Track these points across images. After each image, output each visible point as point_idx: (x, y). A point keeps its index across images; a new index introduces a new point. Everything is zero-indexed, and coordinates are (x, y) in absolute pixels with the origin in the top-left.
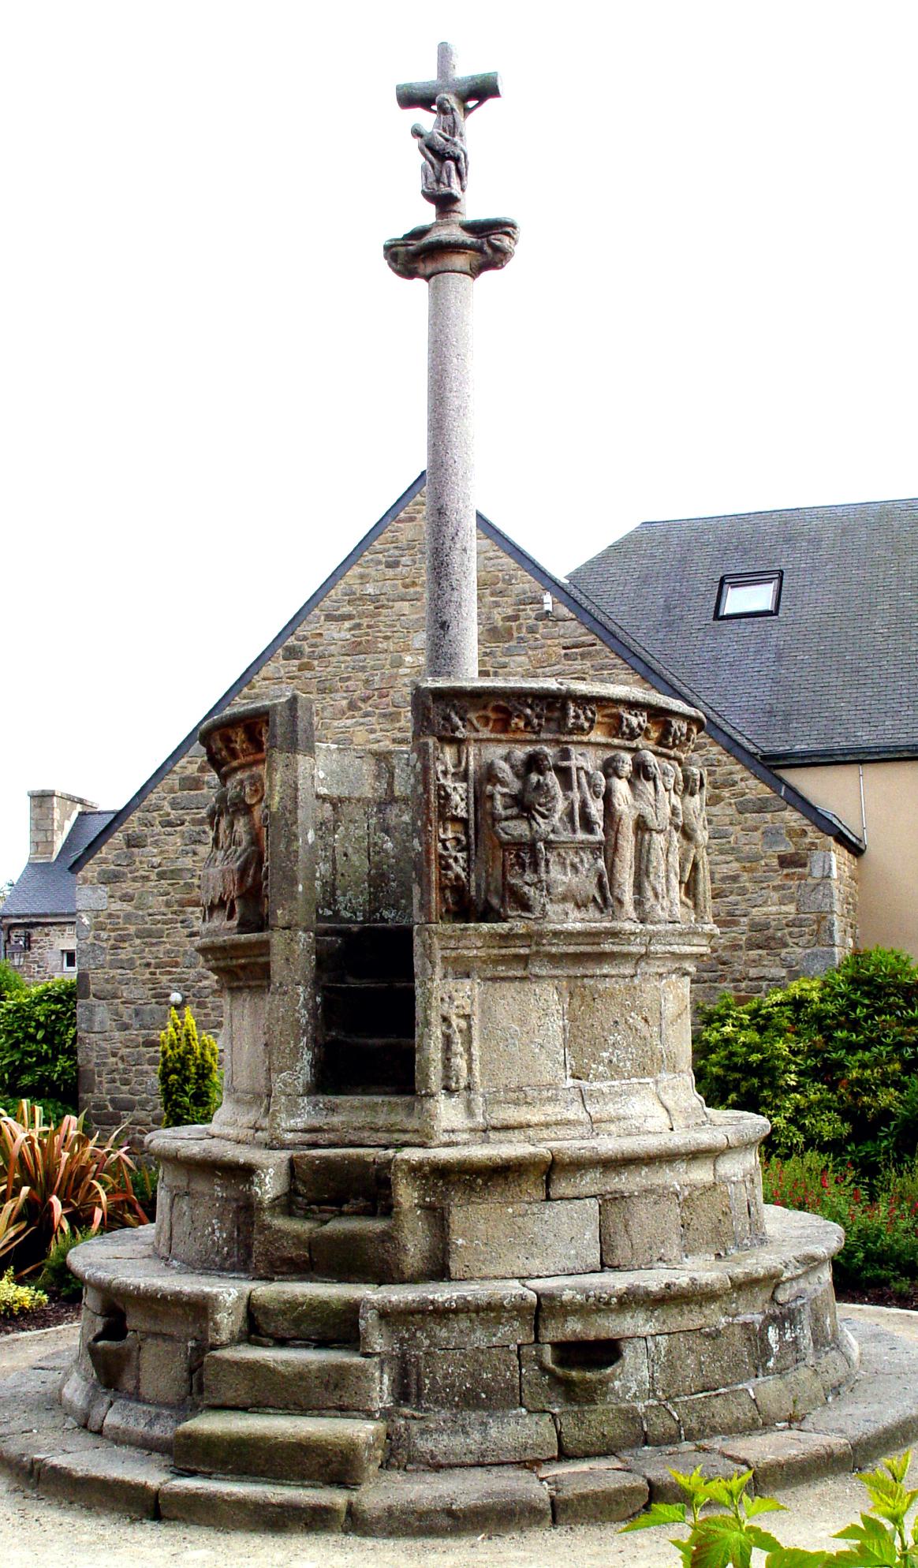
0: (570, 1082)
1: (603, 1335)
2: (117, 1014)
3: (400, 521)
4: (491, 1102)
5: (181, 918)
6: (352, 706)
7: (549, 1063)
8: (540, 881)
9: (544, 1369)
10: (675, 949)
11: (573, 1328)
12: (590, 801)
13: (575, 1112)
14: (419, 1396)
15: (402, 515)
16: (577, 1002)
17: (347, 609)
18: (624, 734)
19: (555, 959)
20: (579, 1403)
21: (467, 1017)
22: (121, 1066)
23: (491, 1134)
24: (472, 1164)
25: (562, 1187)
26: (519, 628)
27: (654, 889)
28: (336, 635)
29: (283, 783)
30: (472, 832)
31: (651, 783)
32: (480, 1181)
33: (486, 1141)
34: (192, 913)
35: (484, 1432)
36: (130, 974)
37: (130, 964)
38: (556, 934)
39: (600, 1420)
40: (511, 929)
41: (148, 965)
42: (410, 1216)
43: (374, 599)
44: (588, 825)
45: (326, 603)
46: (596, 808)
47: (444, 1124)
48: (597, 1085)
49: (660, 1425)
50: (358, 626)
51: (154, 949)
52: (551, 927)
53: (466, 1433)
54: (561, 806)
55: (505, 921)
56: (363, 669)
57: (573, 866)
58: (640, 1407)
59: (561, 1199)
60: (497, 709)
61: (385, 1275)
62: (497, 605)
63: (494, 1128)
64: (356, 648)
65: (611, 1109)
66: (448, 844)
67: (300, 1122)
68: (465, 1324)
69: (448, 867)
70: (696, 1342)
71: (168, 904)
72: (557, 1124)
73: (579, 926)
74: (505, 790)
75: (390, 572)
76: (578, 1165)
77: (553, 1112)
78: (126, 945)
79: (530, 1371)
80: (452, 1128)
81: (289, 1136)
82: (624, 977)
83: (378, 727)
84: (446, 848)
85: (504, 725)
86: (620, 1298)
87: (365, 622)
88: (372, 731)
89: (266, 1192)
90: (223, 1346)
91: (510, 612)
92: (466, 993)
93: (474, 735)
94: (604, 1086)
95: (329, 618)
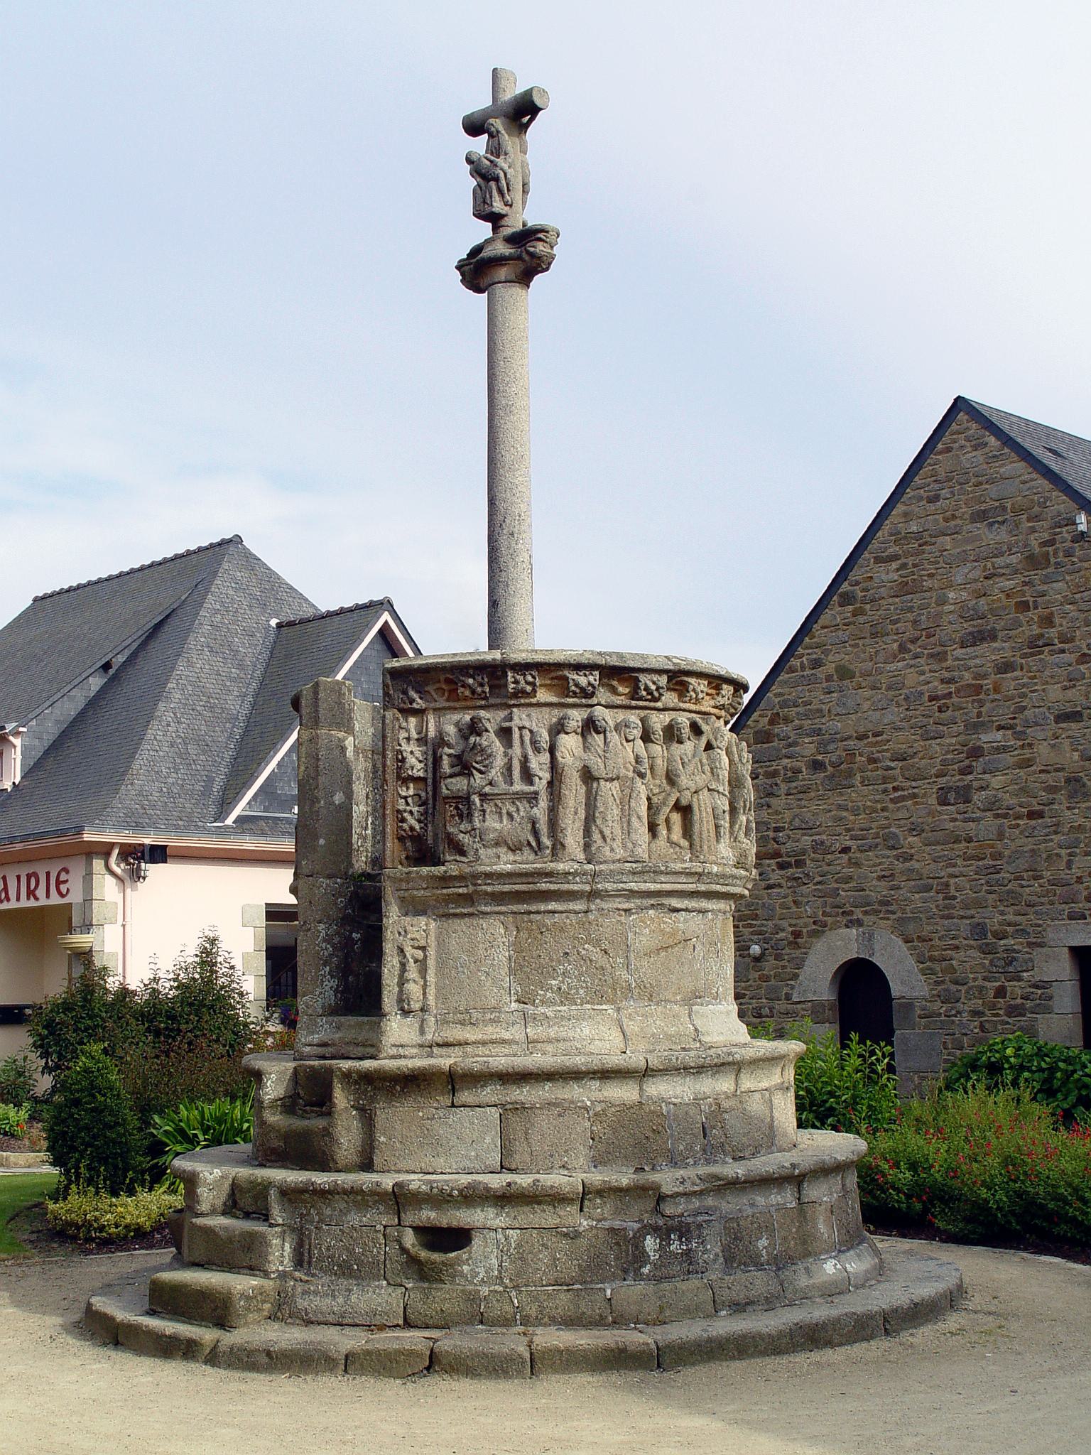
0: (514, 1006)
1: (455, 1224)
3: (940, 453)
4: (443, 1022)
6: (903, 649)
7: (498, 988)
9: (403, 1250)
10: (633, 886)
11: (429, 1216)
13: (515, 1032)
14: (309, 1263)
15: (940, 446)
16: (524, 935)
18: (574, 692)
19: (500, 898)
20: (429, 1281)
21: (423, 949)
23: (435, 1050)
24: (385, 1072)
25: (465, 1096)
26: (1055, 553)
27: (601, 832)
28: (884, 577)
29: (308, 755)
30: (430, 789)
32: (398, 1088)
33: (430, 1055)
34: (769, 866)
35: (347, 1298)
38: (489, 875)
39: (444, 1298)
42: (344, 1116)
43: (918, 536)
44: (528, 776)
45: (874, 545)
46: (539, 763)
47: (392, 1040)
48: (542, 1010)
49: (498, 1309)
50: (904, 566)
52: (481, 869)
53: (334, 1297)
54: (499, 761)
56: (910, 610)
57: (510, 815)
58: (485, 1291)
59: (464, 1106)
60: (448, 681)
61: (324, 1164)
62: (1033, 530)
63: (438, 1045)
64: (904, 589)
65: (553, 1032)
66: (410, 800)
67: (316, 1038)
68: (343, 1205)
69: (403, 820)
70: (551, 1240)
72: (493, 1042)
74: (452, 751)
77: (491, 1032)
79: (392, 1249)
80: (400, 1040)
81: (308, 1049)
82: (576, 912)
83: (926, 668)
84: (408, 804)
85: (453, 695)
86: (461, 1191)
87: (910, 561)
88: (923, 673)
89: (267, 1094)
90: (202, 1215)
91: (1046, 536)
92: (423, 928)
93: (432, 705)
94: (548, 1011)
95: (878, 560)
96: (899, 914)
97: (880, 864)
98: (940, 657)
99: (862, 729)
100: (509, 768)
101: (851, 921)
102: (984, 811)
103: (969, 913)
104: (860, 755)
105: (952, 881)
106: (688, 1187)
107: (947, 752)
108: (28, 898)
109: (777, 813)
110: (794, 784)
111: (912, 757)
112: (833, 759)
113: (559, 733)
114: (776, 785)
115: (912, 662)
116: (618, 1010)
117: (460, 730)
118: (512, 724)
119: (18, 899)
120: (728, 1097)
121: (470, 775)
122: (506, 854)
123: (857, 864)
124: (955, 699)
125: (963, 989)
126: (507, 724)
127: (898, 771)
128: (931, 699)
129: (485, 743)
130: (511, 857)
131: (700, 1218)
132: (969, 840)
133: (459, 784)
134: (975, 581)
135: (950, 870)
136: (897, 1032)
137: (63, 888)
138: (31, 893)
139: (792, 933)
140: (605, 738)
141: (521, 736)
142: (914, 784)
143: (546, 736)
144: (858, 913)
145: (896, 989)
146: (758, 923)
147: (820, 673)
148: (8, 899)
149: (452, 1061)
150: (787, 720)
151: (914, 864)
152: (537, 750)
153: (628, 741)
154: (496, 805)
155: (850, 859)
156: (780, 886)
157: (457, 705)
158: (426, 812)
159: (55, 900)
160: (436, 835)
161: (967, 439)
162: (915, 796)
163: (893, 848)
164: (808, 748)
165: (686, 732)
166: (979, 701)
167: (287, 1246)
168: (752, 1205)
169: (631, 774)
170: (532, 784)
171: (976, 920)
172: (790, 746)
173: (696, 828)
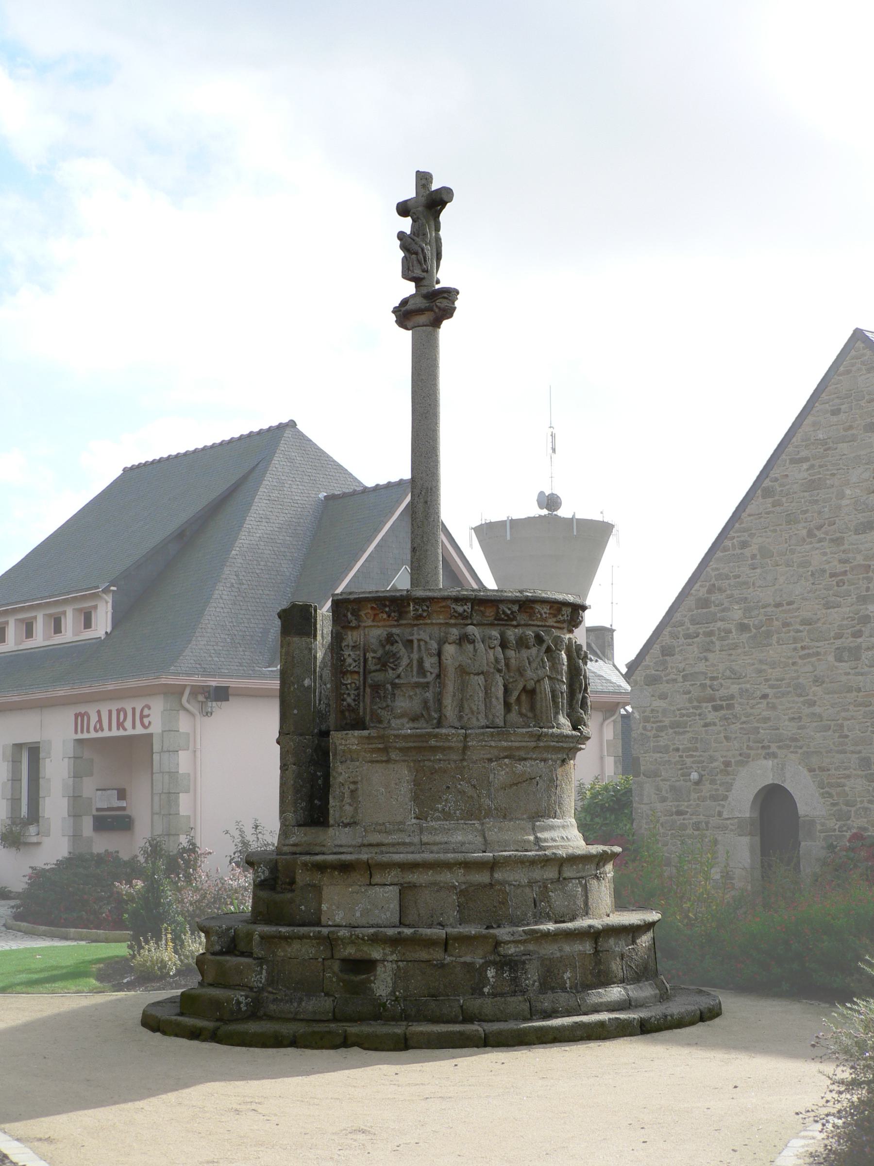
0: (414, 821)
2: (658, 790)
5: (698, 712)
6: (810, 534)
11: (350, 951)
12: (425, 658)
15: (842, 369)
17: (804, 453)
22: (662, 831)
30: (362, 679)
31: (472, 646)
34: (706, 707)
35: (300, 1003)
36: (666, 757)
37: (665, 750)
38: (396, 736)
41: (678, 750)
43: (824, 442)
44: (422, 671)
45: (790, 449)
46: (429, 663)
48: (433, 824)
51: (681, 737)
52: (392, 732)
63: (364, 845)
64: (812, 485)
65: (438, 839)
69: (344, 700)
71: (690, 701)
72: (399, 844)
75: (834, 419)
76: (386, 866)
78: (663, 734)
95: (793, 461)
96: (805, 749)
97: (791, 708)
98: (837, 541)
99: (778, 599)
101: (768, 754)
102: (870, 667)
103: (858, 748)
104: (777, 619)
105: (846, 723)
106: (517, 938)
107: (843, 619)
108: (118, 729)
109: (713, 665)
110: (726, 642)
111: (816, 622)
112: (756, 622)
113: (445, 643)
114: (712, 642)
115: (818, 545)
116: (482, 824)
119: (110, 729)
120: (552, 883)
121: (386, 670)
123: (774, 707)
124: (850, 576)
125: (853, 809)
126: (410, 638)
127: (805, 633)
128: (832, 575)
130: (411, 725)
131: (524, 958)
132: (859, 690)
134: (867, 480)
135: (843, 714)
136: (803, 844)
137: (146, 721)
138: (120, 725)
139: (723, 763)
140: (475, 647)
141: (419, 646)
142: (817, 644)
144: (774, 748)
145: (802, 809)
146: (697, 754)
147: (747, 552)
148: (102, 730)
149: (370, 856)
150: (720, 590)
151: (817, 709)
153: (490, 648)
155: (768, 704)
156: (715, 724)
158: (358, 695)
159: (139, 730)
161: (863, 363)
162: (818, 654)
163: (800, 695)
164: (737, 613)
165: (532, 641)
166: (867, 578)
167: (264, 972)
168: (560, 950)
169: (492, 670)
170: (425, 676)
171: (863, 755)
172: (723, 610)
173: (538, 706)
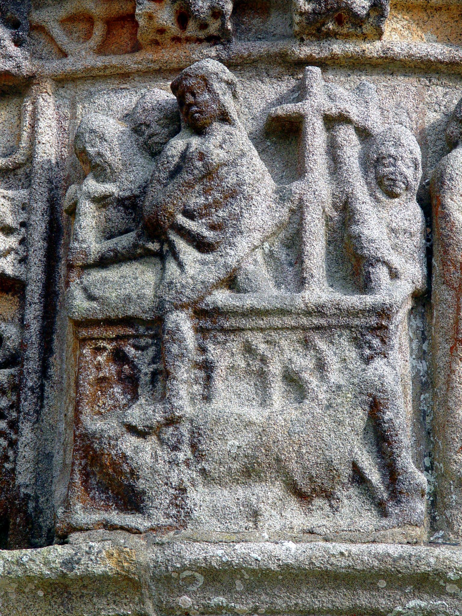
8: (172, 421)
40: (69, 563)
44: (353, 263)
54: (261, 215)
55: (63, 540)
73: (290, 551)
74: (110, 188)
93: (55, 66)
100: (293, 240)
117: (137, 130)
118: (306, 107)
122: (279, 506)
126: (290, 108)
129: (218, 155)
130: (296, 516)
133: (133, 284)
141: (333, 150)
143: (412, 148)
152: (386, 187)
154: (249, 350)
157: (130, 61)
160: (44, 458)
170: (365, 285)
